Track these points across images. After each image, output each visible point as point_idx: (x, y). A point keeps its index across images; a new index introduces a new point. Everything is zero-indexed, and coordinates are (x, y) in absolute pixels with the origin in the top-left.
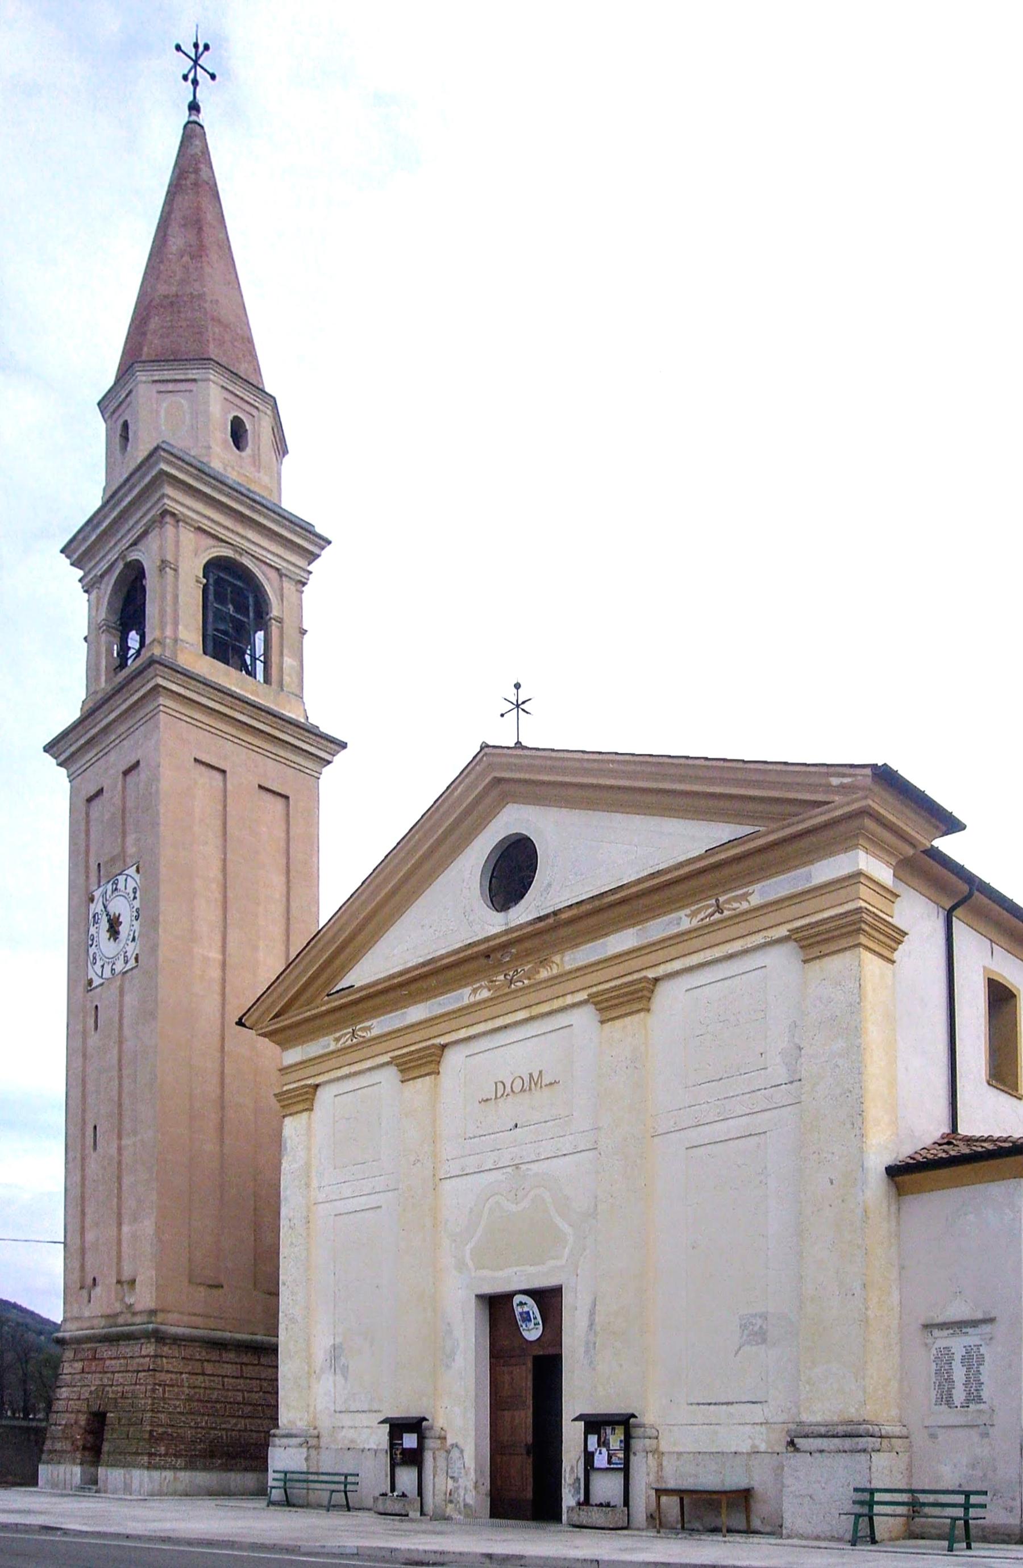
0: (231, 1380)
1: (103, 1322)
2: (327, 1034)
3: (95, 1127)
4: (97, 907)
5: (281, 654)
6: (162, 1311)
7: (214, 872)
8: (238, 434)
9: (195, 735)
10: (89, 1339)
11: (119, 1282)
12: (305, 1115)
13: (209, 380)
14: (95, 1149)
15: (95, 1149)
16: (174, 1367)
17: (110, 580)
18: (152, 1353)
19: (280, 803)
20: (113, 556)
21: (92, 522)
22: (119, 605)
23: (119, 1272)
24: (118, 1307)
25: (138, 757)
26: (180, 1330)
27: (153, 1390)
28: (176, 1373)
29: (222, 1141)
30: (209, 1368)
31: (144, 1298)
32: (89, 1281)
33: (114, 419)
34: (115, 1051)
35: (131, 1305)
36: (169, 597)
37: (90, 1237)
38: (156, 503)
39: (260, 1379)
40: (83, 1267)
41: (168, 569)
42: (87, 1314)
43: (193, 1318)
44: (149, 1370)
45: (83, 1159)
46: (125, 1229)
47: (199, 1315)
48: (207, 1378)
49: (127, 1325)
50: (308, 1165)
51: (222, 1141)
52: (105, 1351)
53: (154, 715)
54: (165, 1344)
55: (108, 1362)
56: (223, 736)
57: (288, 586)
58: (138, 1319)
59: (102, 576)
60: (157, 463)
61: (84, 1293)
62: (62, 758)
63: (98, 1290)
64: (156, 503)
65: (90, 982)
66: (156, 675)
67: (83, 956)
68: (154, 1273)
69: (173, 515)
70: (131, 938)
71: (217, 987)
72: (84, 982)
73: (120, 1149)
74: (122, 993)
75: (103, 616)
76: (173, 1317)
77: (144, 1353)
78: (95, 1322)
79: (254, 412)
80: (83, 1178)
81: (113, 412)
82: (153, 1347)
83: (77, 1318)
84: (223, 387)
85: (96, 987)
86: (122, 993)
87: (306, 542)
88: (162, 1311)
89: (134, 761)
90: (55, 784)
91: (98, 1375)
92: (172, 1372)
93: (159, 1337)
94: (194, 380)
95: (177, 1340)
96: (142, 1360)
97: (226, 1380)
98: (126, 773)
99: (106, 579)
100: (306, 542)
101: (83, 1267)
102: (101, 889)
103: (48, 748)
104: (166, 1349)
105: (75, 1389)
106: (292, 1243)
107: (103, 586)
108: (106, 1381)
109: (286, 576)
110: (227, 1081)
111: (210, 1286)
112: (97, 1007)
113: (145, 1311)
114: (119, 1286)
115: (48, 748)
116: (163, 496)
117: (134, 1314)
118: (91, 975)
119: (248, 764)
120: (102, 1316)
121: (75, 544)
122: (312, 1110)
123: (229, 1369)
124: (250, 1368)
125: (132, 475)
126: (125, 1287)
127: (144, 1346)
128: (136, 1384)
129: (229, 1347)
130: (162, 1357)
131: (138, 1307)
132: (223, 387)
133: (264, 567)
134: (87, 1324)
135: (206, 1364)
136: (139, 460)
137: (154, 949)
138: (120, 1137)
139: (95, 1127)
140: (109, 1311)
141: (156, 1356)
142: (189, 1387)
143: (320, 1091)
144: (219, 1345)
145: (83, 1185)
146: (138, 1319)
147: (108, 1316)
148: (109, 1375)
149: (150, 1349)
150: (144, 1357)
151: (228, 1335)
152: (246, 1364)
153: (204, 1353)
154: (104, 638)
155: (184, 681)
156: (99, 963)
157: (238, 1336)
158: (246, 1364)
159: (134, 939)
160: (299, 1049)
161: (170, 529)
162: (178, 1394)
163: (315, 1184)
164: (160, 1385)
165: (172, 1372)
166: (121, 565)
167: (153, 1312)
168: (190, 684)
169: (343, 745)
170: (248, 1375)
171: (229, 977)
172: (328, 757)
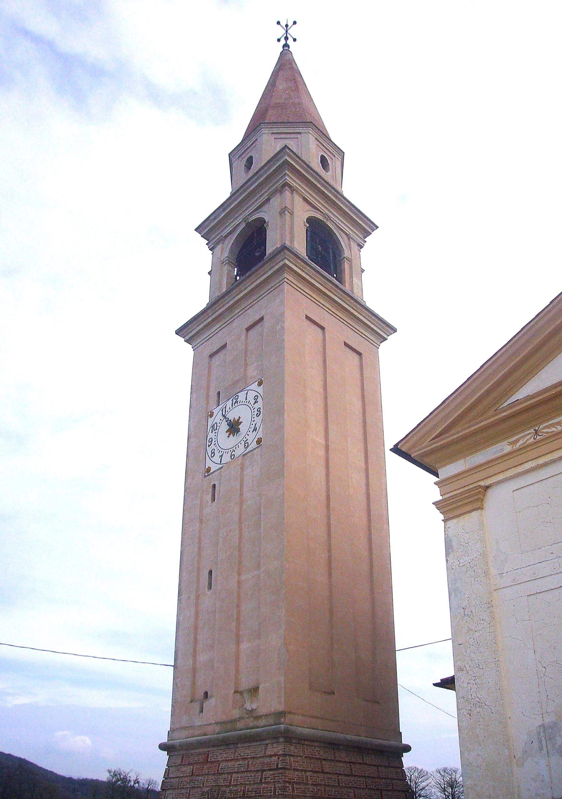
0: (344, 778)
1: (217, 729)
2: (503, 440)
3: (210, 572)
4: (218, 417)
5: (351, 277)
6: (290, 713)
7: (319, 387)
8: (324, 162)
9: (305, 302)
10: (201, 744)
11: (236, 692)
12: (475, 514)
13: (309, 133)
14: (210, 587)
15: (210, 587)
16: (300, 766)
17: (231, 238)
18: (281, 753)
19: (356, 357)
20: (240, 219)
21: (223, 207)
22: (237, 252)
23: (237, 683)
24: (236, 713)
25: (263, 313)
26: (306, 731)
27: (284, 788)
28: (302, 771)
29: (330, 574)
30: (327, 766)
31: (269, 702)
32: (200, 694)
33: (240, 159)
34: (236, 510)
35: (252, 710)
36: (287, 227)
37: (202, 658)
38: (282, 177)
39: (365, 777)
40: (194, 684)
41: (286, 212)
42: (198, 722)
43: (315, 720)
44: (277, 769)
45: (198, 597)
46: (244, 646)
47: (317, 718)
48: (325, 775)
49: (248, 729)
50: (484, 555)
51: (330, 574)
52: (219, 755)
53: (281, 283)
54: (291, 743)
55: (223, 765)
56: (322, 306)
57: (353, 245)
58: (262, 722)
59: (226, 237)
60: (282, 157)
61: (196, 706)
62: (187, 338)
63: (211, 702)
64: (282, 177)
65: (209, 470)
66: (285, 258)
67: (203, 453)
68: (282, 678)
69: (290, 187)
70: (253, 427)
71: (322, 462)
72: (202, 470)
73: (239, 583)
74: (242, 469)
75: (226, 255)
76: (298, 719)
77: (269, 752)
78: (210, 729)
79: (333, 157)
80: (197, 613)
81: (240, 156)
82: (281, 747)
83: (185, 728)
84: (316, 139)
85: (214, 472)
86: (242, 469)
87: (365, 227)
88: (290, 713)
89: (257, 317)
90: (185, 352)
91: (211, 777)
92: (297, 770)
93: (288, 737)
94: (300, 133)
95: (302, 740)
96: (267, 760)
97: (340, 777)
98: (248, 329)
99: (227, 240)
100: (365, 227)
101: (194, 684)
102: (220, 407)
103: (178, 332)
104: (292, 748)
105: (183, 791)
106: (470, 630)
107: (226, 242)
108: (221, 782)
109: (352, 239)
110: (332, 529)
111: (325, 693)
112: (214, 486)
113: (270, 715)
114: (238, 695)
115: (178, 332)
116: (286, 174)
117: (257, 718)
118: (209, 464)
119: (338, 330)
120: (216, 723)
121: (207, 223)
122: (482, 509)
123: (341, 768)
124: (358, 766)
125: (259, 171)
126: (246, 695)
127: (269, 746)
128: (261, 782)
129: (341, 747)
130: (289, 755)
131: (262, 711)
132: (316, 139)
133: (342, 233)
134: (197, 732)
135: (324, 762)
136: (262, 165)
137: (280, 429)
138: (239, 574)
139: (210, 572)
140: (224, 718)
141: (284, 755)
142: (312, 785)
143: (490, 492)
144: (333, 745)
145: (196, 618)
146: (262, 722)
147: (224, 723)
148: (223, 776)
149: (279, 749)
150: (271, 756)
151: (342, 736)
152: (354, 763)
153: (322, 753)
154: (226, 268)
155: (303, 267)
156: (217, 455)
157: (349, 737)
158: (354, 763)
159: (255, 429)
160: (462, 461)
161: (287, 193)
162: (304, 792)
163: (493, 571)
164: (289, 783)
165: (297, 770)
166: (243, 225)
167: (282, 714)
168: (305, 268)
169: (395, 330)
170: (356, 774)
171: (331, 456)
172: (385, 336)
